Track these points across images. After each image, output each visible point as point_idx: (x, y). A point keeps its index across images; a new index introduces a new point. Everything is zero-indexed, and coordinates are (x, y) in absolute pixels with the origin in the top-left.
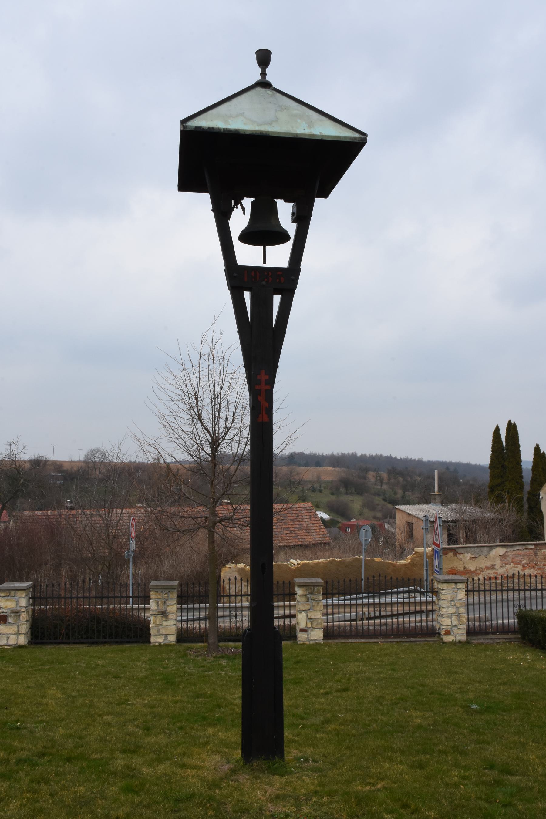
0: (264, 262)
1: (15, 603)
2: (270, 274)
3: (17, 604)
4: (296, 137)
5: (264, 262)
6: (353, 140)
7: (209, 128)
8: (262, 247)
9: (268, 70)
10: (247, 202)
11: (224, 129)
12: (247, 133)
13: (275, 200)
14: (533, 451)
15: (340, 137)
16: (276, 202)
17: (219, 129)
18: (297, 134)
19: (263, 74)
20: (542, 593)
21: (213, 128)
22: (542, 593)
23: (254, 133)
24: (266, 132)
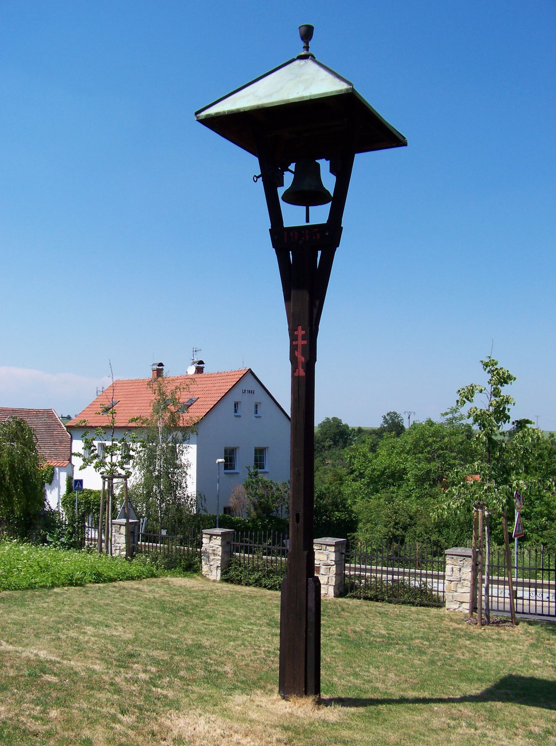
0: (308, 221)
1: (326, 556)
2: (307, 232)
3: (327, 558)
4: (287, 103)
5: (308, 221)
6: (339, 92)
7: (216, 113)
8: (305, 208)
9: (310, 44)
10: (292, 167)
11: (228, 111)
12: (246, 110)
13: (316, 161)
14: (530, 420)
15: (327, 93)
16: (318, 165)
17: (224, 112)
18: (288, 100)
19: (307, 48)
20: (529, 602)
21: (219, 113)
22: (529, 602)
23: (252, 108)
24: (262, 105)
